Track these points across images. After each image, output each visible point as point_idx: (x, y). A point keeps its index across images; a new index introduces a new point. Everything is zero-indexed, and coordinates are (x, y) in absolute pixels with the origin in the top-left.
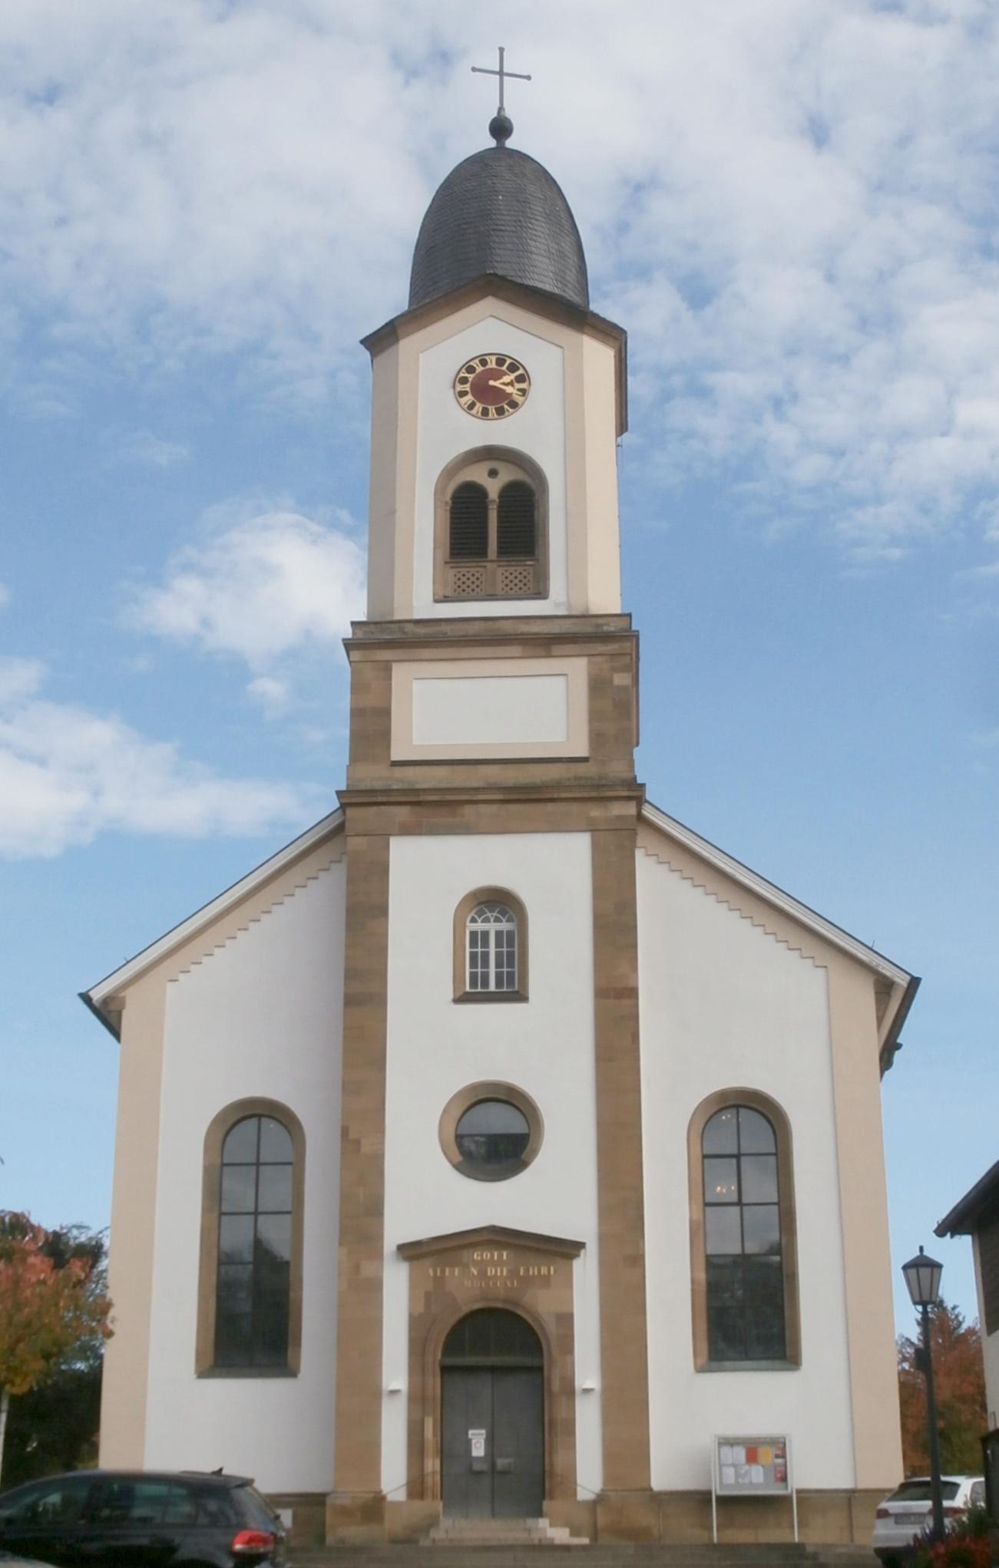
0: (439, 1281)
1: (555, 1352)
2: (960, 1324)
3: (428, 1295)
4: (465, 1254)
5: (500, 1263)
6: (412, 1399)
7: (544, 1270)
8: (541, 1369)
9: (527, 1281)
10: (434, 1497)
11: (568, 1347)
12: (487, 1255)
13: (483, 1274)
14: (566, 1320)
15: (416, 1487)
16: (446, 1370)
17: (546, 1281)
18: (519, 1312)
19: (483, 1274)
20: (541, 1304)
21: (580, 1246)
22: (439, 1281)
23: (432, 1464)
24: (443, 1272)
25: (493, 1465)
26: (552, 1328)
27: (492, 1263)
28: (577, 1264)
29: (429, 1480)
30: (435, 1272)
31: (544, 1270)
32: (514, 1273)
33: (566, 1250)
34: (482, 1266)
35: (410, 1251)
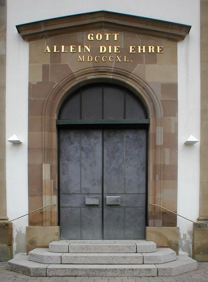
0: (56, 56)
1: (160, 113)
2: (24, 234)
3: (45, 68)
4: (79, 35)
5: (112, 42)
6: (31, 150)
7: (151, 49)
8: (145, 127)
9: (136, 57)
10: (52, 224)
11: (171, 107)
12: (99, 37)
13: (95, 52)
14: (171, 89)
15: (36, 219)
16: (62, 129)
17: (152, 58)
18: (129, 82)
19: (95, 52)
20: (148, 77)
21: (188, 28)
22: (56, 56)
23: (50, 201)
24: (59, 49)
25: (103, 200)
26: (158, 95)
27: (103, 42)
28: (181, 47)
29: (5, 217)
30: (52, 49)
31: (151, 49)
32: (123, 51)
33: (175, 32)
34: (95, 45)
35: (30, 32)
